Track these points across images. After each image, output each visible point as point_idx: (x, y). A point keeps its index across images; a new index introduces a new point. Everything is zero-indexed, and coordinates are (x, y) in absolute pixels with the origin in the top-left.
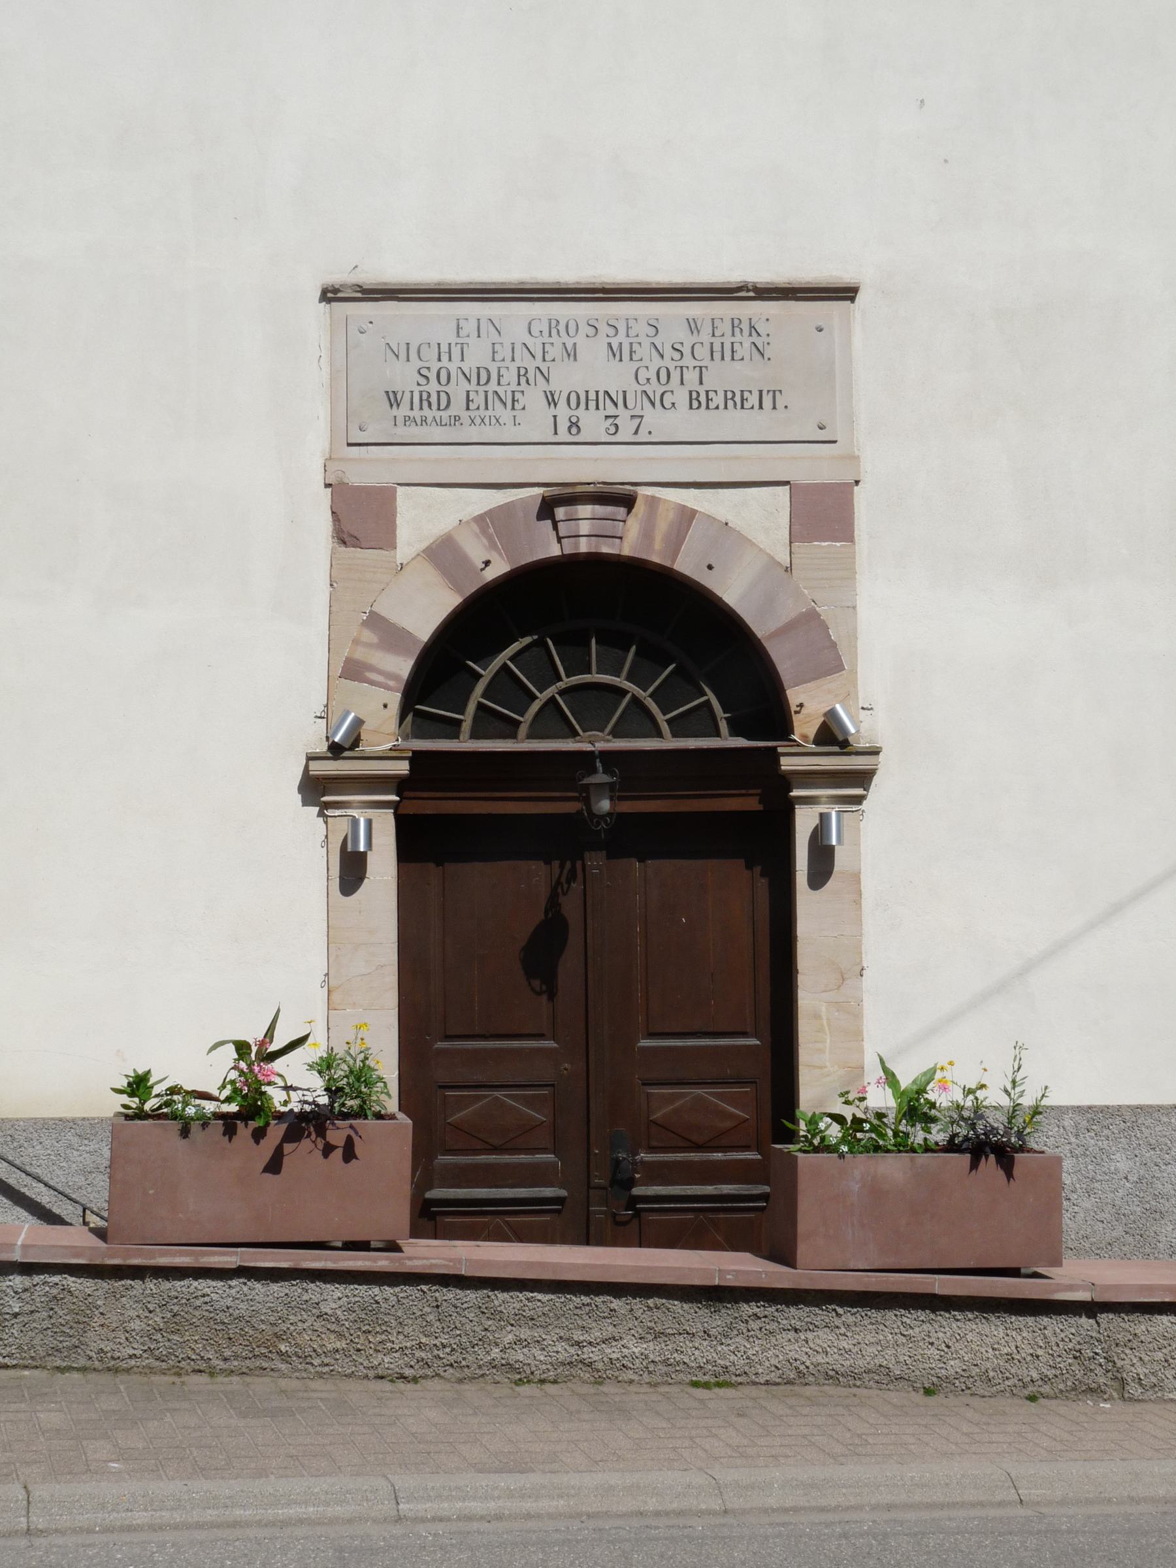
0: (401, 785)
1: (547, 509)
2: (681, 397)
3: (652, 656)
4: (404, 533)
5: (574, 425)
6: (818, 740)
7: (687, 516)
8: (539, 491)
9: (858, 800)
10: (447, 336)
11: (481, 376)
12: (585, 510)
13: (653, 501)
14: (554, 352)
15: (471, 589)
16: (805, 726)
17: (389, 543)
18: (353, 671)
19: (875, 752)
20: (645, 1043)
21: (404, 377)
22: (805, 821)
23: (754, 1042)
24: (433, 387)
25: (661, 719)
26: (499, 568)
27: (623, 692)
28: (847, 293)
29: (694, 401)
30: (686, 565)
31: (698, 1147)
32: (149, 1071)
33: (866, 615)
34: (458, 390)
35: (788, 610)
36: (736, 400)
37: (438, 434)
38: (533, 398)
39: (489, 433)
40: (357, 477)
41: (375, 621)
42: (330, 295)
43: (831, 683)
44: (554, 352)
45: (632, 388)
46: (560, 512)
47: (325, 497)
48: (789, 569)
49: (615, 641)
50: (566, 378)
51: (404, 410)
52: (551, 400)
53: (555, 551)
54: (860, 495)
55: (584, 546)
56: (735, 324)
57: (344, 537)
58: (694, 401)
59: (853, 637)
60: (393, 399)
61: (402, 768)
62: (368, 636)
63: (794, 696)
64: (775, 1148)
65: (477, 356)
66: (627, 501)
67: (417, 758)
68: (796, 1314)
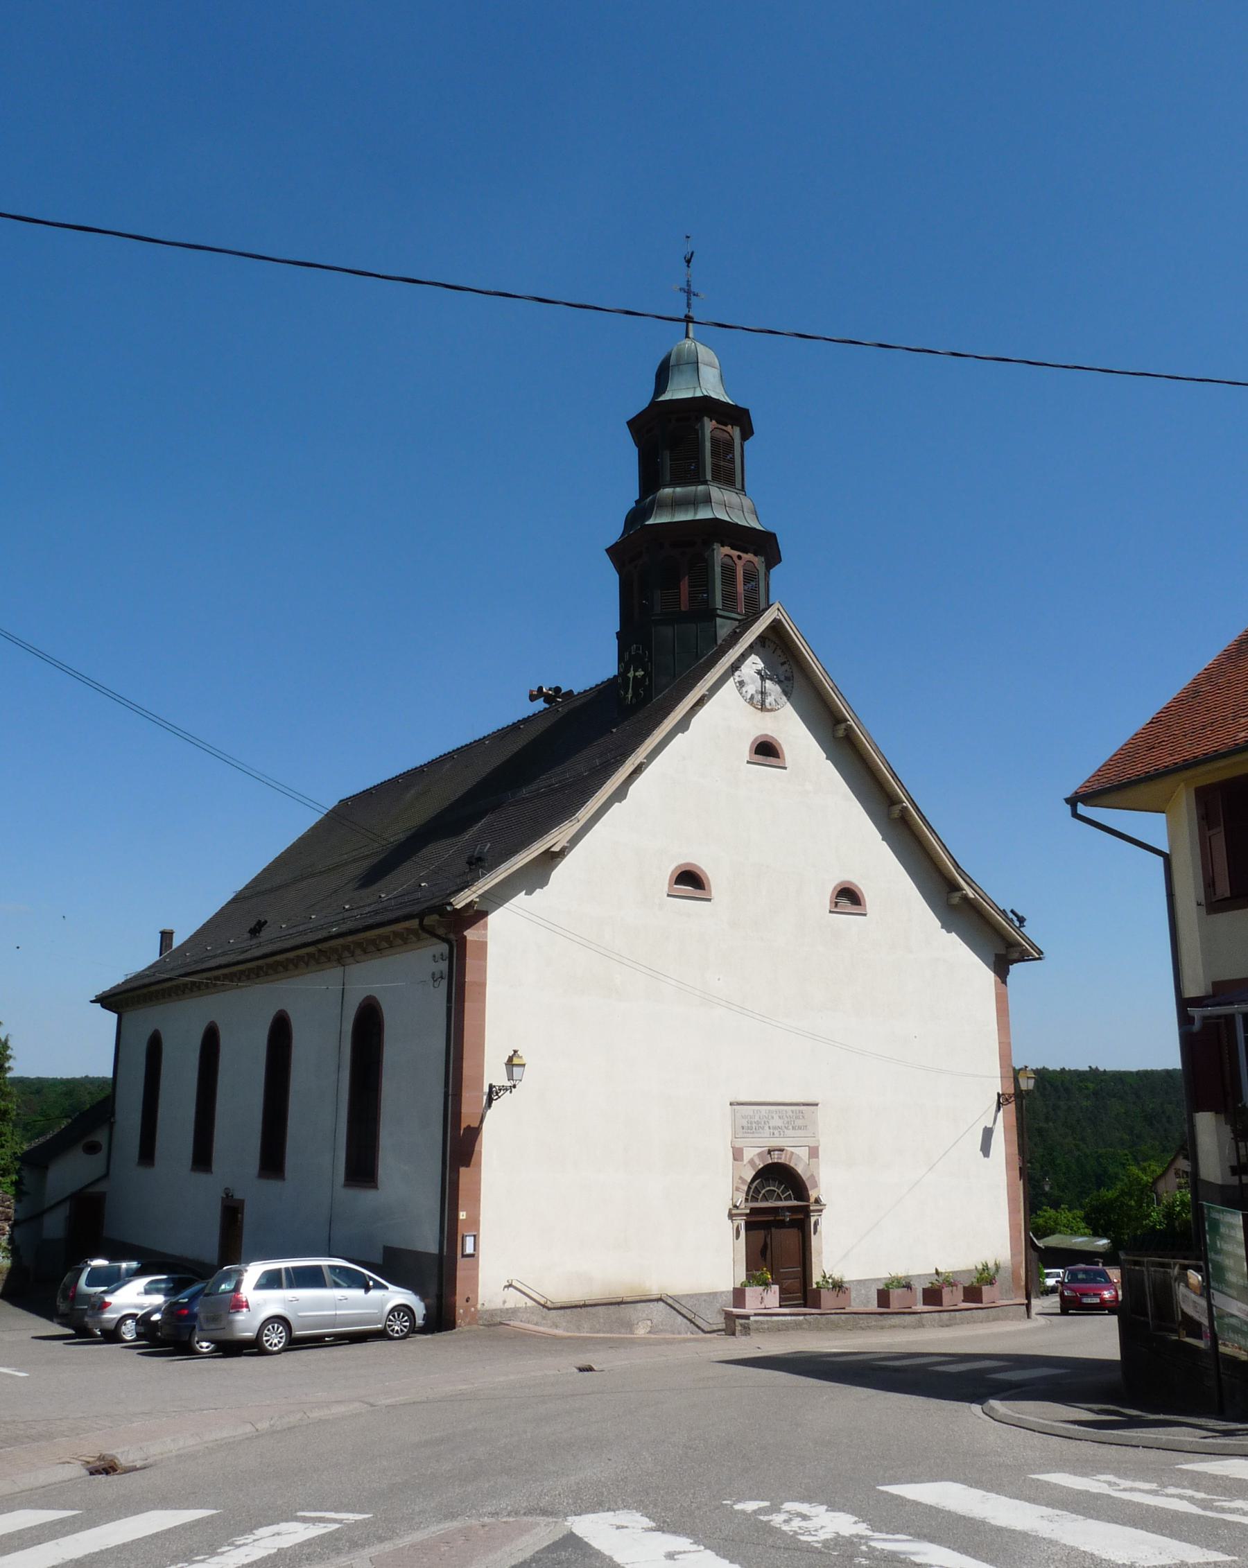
0: (747, 1215)
1: (769, 1152)
2: (791, 1127)
3: (781, 1183)
4: (745, 1158)
5: (773, 1134)
6: (815, 1203)
7: (792, 1153)
8: (767, 1148)
9: (820, 1215)
10: (752, 1114)
11: (758, 1123)
12: (776, 1152)
13: (787, 1150)
14: (770, 1117)
15: (757, 1170)
16: (812, 1200)
17: (742, 1160)
18: (737, 1189)
19: (825, 1205)
20: (782, 1270)
21: (745, 1124)
22: (813, 1220)
23: (799, 1269)
24: (749, 1125)
25: (783, 1197)
26: (761, 1166)
27: (775, 1191)
28: (817, 1105)
29: (793, 1128)
30: (792, 1165)
31: (790, 1293)
32: (255, 1289)
33: (821, 1175)
34: (754, 1125)
35: (809, 1174)
36: (800, 1128)
37: (751, 1135)
38: (766, 1128)
39: (760, 1135)
40: (737, 1146)
41: (741, 1178)
42: (731, 1104)
43: (816, 1190)
44: (770, 1117)
45: (783, 1125)
46: (772, 1153)
47: (731, 1149)
48: (809, 1164)
49: (774, 1180)
50: (772, 1123)
51: (744, 1131)
52: (769, 1128)
53: (771, 1162)
54: (820, 1148)
55: (776, 1161)
56: (799, 1111)
57: (735, 1159)
58: (793, 1128)
59: (819, 1179)
60: (743, 1128)
61: (748, 1211)
62: (740, 1181)
63: (810, 1193)
64: (146, 1341)
65: (757, 1119)
66: (782, 1150)
67: (752, 1209)
68: (890, 1316)
